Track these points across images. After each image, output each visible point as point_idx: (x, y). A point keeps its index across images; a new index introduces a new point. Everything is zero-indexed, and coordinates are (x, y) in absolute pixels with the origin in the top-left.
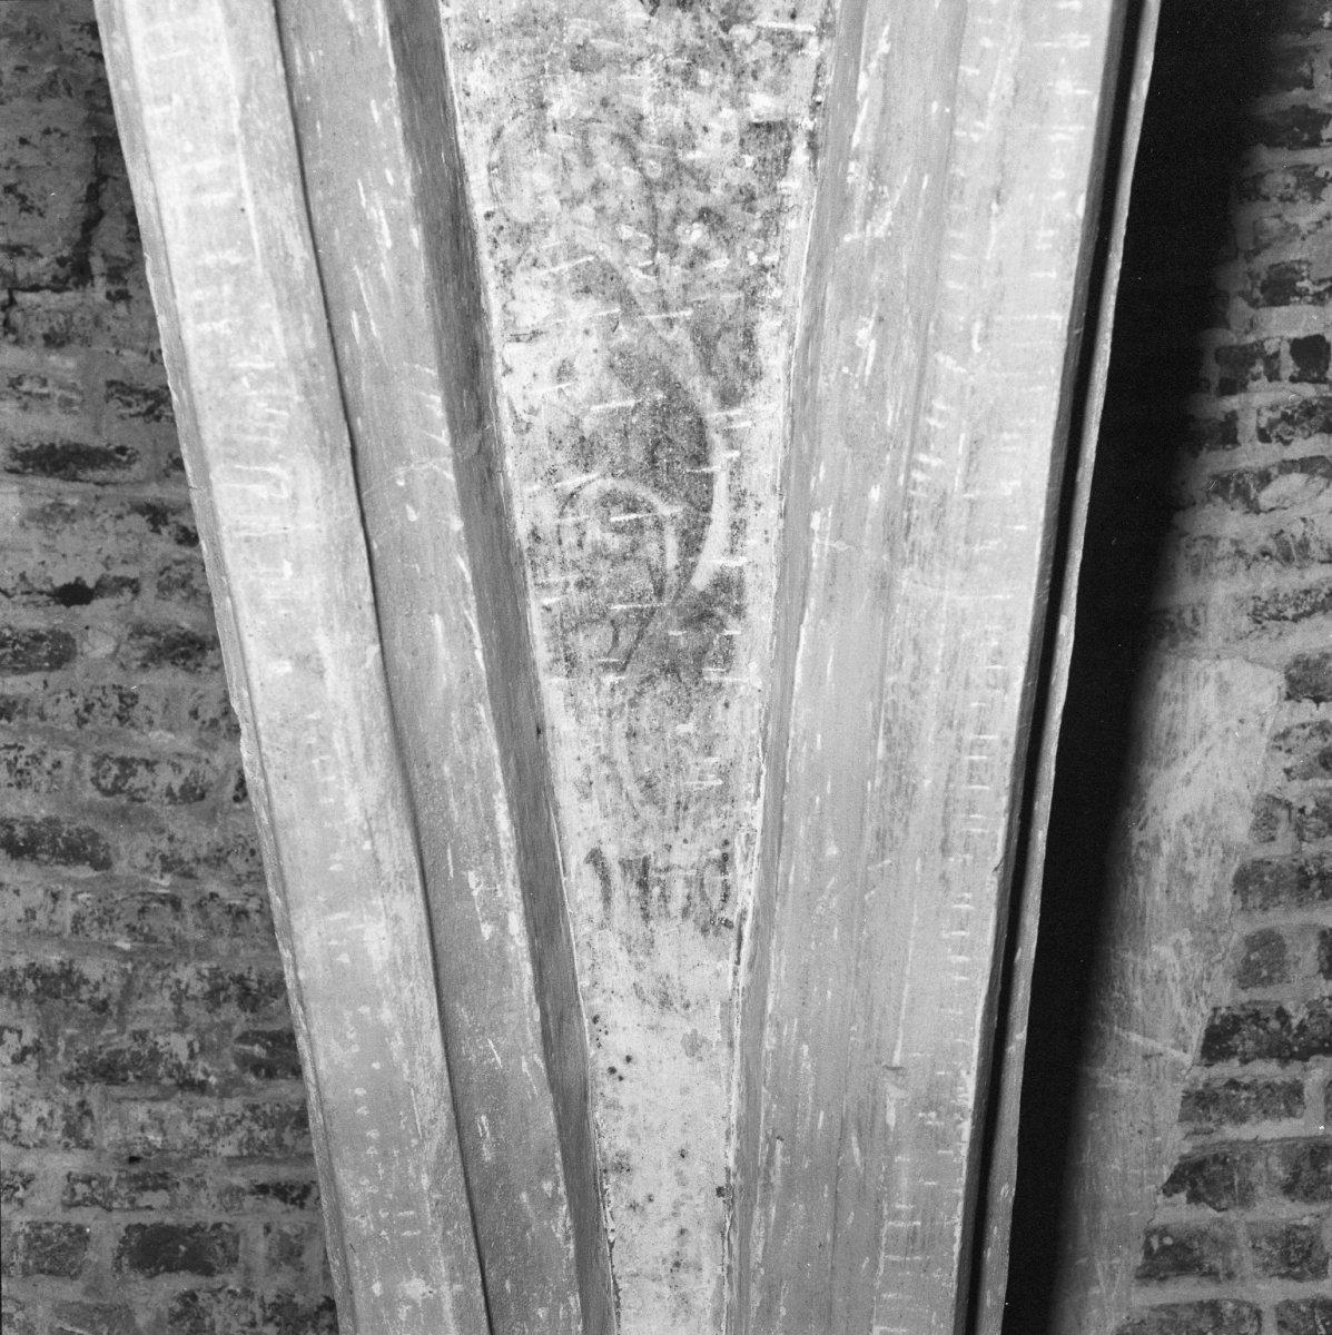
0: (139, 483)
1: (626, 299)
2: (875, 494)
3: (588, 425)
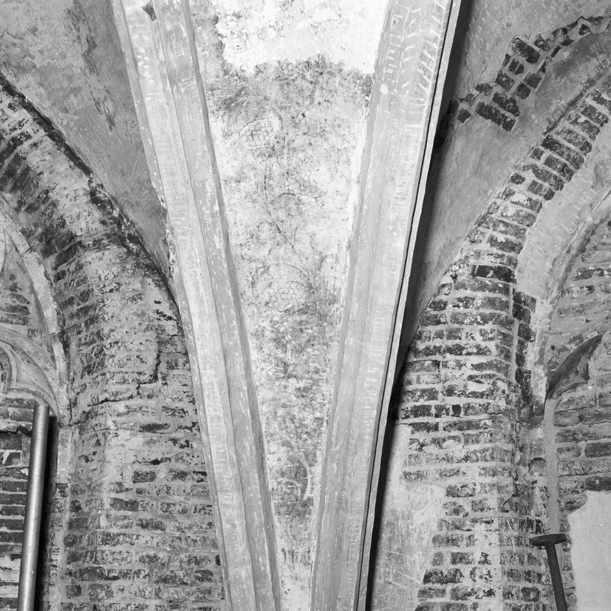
0: (170, 433)
1: (291, 447)
2: (336, 493)
3: (283, 470)
